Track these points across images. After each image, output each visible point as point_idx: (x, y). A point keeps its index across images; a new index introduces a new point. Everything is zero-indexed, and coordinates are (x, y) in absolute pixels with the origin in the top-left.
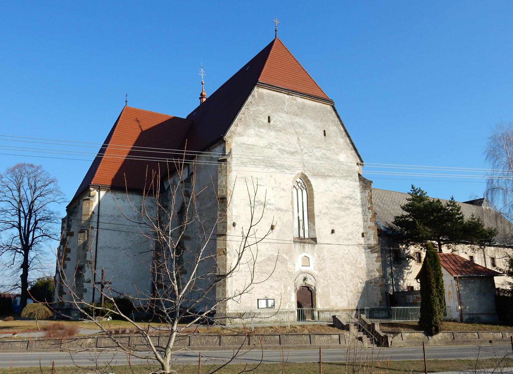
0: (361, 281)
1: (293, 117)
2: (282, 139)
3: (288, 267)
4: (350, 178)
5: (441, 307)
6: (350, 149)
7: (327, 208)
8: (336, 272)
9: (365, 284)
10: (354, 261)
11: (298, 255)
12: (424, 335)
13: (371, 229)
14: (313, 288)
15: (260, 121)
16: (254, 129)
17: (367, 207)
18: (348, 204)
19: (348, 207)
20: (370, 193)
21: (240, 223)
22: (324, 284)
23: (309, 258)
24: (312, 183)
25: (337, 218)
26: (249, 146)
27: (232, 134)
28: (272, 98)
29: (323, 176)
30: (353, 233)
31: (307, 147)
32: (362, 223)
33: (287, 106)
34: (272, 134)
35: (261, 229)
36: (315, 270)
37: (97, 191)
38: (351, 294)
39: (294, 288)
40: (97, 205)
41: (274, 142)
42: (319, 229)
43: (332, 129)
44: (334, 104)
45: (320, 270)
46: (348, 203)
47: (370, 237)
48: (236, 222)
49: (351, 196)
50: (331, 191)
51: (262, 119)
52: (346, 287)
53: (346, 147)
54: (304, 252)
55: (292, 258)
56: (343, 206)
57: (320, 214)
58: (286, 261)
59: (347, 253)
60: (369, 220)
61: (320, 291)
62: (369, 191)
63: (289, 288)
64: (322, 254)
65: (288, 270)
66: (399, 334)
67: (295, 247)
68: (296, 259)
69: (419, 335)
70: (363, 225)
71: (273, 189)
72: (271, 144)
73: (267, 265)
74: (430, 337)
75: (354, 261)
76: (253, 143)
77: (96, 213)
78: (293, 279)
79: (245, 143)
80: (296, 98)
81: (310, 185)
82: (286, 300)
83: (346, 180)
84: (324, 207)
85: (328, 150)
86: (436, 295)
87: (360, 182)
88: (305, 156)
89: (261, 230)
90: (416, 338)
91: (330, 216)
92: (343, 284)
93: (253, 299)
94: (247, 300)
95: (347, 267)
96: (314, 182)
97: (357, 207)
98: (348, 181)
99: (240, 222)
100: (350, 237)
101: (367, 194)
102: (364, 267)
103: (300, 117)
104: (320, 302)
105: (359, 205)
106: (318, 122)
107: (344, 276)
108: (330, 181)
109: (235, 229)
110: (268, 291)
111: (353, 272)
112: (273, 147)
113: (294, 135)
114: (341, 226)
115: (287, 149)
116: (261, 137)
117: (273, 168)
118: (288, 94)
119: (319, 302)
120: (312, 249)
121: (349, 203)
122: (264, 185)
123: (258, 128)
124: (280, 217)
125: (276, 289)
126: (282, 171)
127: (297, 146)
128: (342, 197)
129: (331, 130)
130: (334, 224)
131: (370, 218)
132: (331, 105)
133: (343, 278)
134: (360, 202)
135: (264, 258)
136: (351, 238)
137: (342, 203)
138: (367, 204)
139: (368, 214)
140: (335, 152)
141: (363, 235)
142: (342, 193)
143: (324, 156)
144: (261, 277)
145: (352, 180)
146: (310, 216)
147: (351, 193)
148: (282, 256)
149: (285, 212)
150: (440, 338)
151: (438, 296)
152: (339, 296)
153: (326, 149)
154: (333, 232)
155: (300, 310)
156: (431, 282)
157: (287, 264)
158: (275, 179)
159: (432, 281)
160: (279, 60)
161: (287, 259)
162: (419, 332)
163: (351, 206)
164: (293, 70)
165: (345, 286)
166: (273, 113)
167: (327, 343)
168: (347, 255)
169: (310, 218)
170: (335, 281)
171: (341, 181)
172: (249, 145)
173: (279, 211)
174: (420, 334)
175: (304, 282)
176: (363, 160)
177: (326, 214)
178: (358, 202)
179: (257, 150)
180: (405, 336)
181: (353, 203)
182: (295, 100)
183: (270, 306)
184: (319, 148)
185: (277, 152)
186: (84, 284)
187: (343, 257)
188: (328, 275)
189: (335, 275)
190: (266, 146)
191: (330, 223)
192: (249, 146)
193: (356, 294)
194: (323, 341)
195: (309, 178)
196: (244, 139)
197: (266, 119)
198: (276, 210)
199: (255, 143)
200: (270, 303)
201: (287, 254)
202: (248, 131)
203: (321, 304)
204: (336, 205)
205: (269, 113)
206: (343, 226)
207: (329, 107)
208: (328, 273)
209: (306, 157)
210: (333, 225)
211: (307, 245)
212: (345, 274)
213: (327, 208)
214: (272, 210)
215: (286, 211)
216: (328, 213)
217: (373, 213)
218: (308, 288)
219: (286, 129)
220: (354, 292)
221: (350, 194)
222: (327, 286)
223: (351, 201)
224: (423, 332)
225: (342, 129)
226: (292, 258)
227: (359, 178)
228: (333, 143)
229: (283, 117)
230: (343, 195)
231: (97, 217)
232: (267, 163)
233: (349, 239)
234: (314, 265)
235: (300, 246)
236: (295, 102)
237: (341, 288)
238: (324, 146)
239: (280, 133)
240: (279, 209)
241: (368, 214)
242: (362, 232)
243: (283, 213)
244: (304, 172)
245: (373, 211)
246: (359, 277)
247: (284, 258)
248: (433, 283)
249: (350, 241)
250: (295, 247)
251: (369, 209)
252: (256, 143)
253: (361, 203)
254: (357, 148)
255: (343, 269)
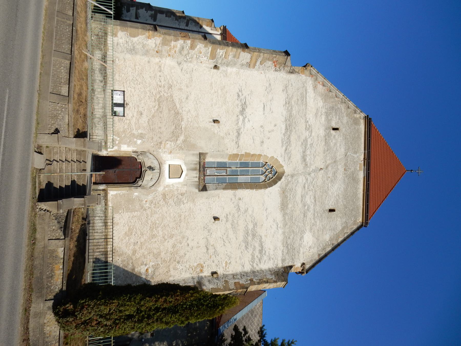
0: (150, 271)
1: (343, 164)
2: (318, 145)
3: (168, 142)
4: (285, 251)
5: (117, 322)
6: (320, 253)
7: (246, 211)
8: (162, 224)
9: (145, 279)
10: (178, 259)
11: (184, 160)
12: (57, 290)
13: (224, 285)
14: (140, 183)
15: (333, 117)
16: (323, 106)
17: (252, 277)
18: (253, 247)
19: (249, 247)
20: (272, 281)
21: (219, 75)
22: (144, 202)
23: (180, 178)
24: (274, 187)
25: (234, 227)
26: (305, 98)
27: (314, 77)
28: (357, 135)
29: (284, 206)
30: (217, 256)
31: (314, 182)
32: (231, 272)
33: (353, 156)
34: (321, 132)
35: (214, 105)
36: (165, 188)
37: (220, 33)
38: (130, 252)
39: (140, 150)
40: (206, 31)
41: (313, 134)
42: (219, 197)
43: (338, 222)
44: (365, 226)
45: (164, 196)
46: (255, 246)
47: (213, 283)
48: (220, 71)
49: (264, 252)
50: (267, 218)
51: (335, 119)
52: (141, 243)
53: (321, 245)
54: (187, 170)
55: (179, 150)
56: (250, 238)
57: (237, 198)
58: (176, 139)
59: (188, 245)
60: (237, 281)
61: (135, 194)
62: (274, 279)
63: (139, 142)
64: (186, 200)
65: (164, 142)
66: (61, 233)
67: (193, 154)
68: (178, 155)
69: (58, 278)
70: (227, 273)
71: (262, 126)
72: (310, 129)
73: (169, 109)
74: (51, 303)
75: (178, 259)
76: (308, 104)
77: (200, 30)
78: (151, 150)
79: (307, 93)
80: (362, 170)
81: (270, 185)
82: (123, 136)
83: (283, 244)
84: (247, 206)
85: (314, 214)
86: (142, 306)
87: (282, 268)
88: (304, 178)
89: (212, 105)
90: (52, 271)
91: (236, 215)
92: (145, 237)
93: (125, 84)
94: (123, 75)
95: (169, 245)
96: (276, 188)
97: (251, 263)
98: (282, 248)
99: (220, 77)
100: (211, 251)
101: (269, 277)
102: (171, 276)
103: (345, 174)
104: (119, 194)
105: (253, 266)
106: (342, 201)
107: (156, 239)
108: (279, 216)
109: (211, 68)
110: (135, 108)
111: (163, 255)
112: (307, 132)
113: (324, 163)
114: (225, 234)
115: (308, 152)
116: (316, 114)
117: (285, 129)
118: (364, 159)
119: (120, 192)
120: (192, 183)
121: (254, 249)
122: (265, 114)
123: (325, 112)
124: (229, 134)
125: (138, 120)
126: (282, 142)
127: (313, 167)
128: (261, 237)
129: (337, 220)
130: (227, 221)
131: (239, 282)
132: (363, 222)
133: (153, 236)
134: (258, 268)
135: (178, 106)
136: (209, 251)
137: (254, 235)
138: (256, 278)
139: (244, 279)
140: (313, 225)
141: (213, 273)
142: (266, 236)
143: (306, 208)
144: (153, 100)
145: (283, 255)
146: (234, 185)
147: (267, 254)
148: (181, 133)
149: (236, 142)
150: (47, 329)
151: (138, 311)
152: (127, 229)
153: (314, 211)
154: (216, 218)
155: (112, 3)
156: (167, 295)
157: (171, 141)
158: (273, 131)
159: (169, 299)
160: (375, 202)
161: (178, 142)
162: (65, 279)
163: (251, 252)
164: (391, 169)
165: (142, 240)
166: (343, 135)
167: (55, 74)
168: (186, 244)
169: (231, 185)
170: (149, 222)
171: (280, 237)
172: (306, 98)
173: (237, 134)
174: (60, 281)
175: (148, 168)
176: (309, 272)
177: (239, 209)
178: (257, 265)
179: (302, 109)
180: (58, 247)
181: (255, 256)
182: (360, 170)
183: (115, 110)
184: (315, 201)
185: (303, 138)
186: (135, 8)
187: (183, 237)
188: (158, 210)
189: (157, 222)
190: (308, 121)
191: (227, 215)
192: (305, 98)
193: (131, 261)
194: (58, 71)
195: (279, 183)
196: (311, 93)
197: (336, 125)
198: (237, 129)
199: (309, 106)
200: (119, 110)
201: (184, 141)
202: (319, 98)
203: (116, 196)
204: (251, 226)
205: (342, 129)
206: (224, 238)
207: (360, 220)
208: (161, 211)
209: (301, 179)
210: (225, 219)
211: (198, 175)
212: (159, 240)
213: (246, 211)
214: (237, 122)
215: (237, 143)
216: (239, 213)
217: (246, 286)
218: (140, 176)
219: (329, 151)
220: (134, 258)
221: (265, 252)
222: (142, 207)
223: (257, 253)
224: (64, 288)
225: (340, 240)
226: (179, 150)
227: (287, 267)
228: (323, 224)
229: (340, 148)
230: (263, 238)
231: (198, 31)
232: (290, 121)
233: (208, 249)
234: (171, 186)
235: (196, 162)
236: (358, 169)
237: (139, 233)
238: (318, 208)
239: (324, 143)
240: (239, 134)
241: (244, 279)
242: (219, 273)
243: (234, 139)
244: (285, 175)
245: (249, 285)
246: (156, 268)
247: (179, 137)
248: (165, 301)
249: (206, 250)
250: (193, 154)
251: (250, 280)
252: (309, 108)
253: (256, 271)
254: (322, 262)
255: (166, 237)
